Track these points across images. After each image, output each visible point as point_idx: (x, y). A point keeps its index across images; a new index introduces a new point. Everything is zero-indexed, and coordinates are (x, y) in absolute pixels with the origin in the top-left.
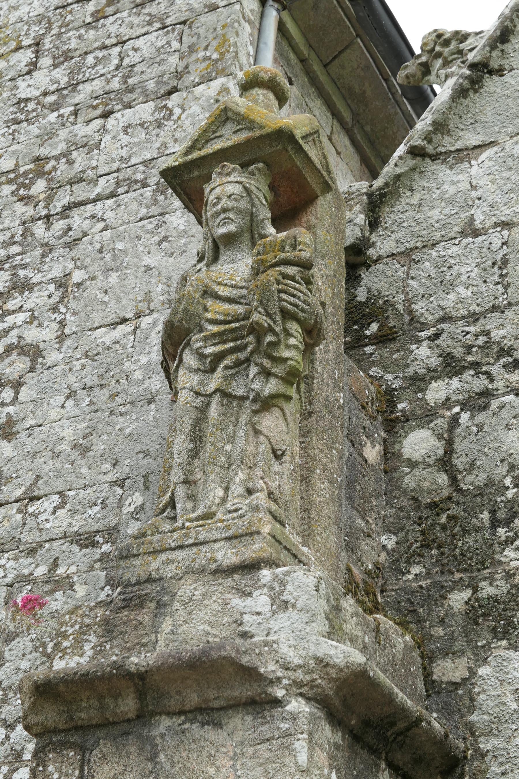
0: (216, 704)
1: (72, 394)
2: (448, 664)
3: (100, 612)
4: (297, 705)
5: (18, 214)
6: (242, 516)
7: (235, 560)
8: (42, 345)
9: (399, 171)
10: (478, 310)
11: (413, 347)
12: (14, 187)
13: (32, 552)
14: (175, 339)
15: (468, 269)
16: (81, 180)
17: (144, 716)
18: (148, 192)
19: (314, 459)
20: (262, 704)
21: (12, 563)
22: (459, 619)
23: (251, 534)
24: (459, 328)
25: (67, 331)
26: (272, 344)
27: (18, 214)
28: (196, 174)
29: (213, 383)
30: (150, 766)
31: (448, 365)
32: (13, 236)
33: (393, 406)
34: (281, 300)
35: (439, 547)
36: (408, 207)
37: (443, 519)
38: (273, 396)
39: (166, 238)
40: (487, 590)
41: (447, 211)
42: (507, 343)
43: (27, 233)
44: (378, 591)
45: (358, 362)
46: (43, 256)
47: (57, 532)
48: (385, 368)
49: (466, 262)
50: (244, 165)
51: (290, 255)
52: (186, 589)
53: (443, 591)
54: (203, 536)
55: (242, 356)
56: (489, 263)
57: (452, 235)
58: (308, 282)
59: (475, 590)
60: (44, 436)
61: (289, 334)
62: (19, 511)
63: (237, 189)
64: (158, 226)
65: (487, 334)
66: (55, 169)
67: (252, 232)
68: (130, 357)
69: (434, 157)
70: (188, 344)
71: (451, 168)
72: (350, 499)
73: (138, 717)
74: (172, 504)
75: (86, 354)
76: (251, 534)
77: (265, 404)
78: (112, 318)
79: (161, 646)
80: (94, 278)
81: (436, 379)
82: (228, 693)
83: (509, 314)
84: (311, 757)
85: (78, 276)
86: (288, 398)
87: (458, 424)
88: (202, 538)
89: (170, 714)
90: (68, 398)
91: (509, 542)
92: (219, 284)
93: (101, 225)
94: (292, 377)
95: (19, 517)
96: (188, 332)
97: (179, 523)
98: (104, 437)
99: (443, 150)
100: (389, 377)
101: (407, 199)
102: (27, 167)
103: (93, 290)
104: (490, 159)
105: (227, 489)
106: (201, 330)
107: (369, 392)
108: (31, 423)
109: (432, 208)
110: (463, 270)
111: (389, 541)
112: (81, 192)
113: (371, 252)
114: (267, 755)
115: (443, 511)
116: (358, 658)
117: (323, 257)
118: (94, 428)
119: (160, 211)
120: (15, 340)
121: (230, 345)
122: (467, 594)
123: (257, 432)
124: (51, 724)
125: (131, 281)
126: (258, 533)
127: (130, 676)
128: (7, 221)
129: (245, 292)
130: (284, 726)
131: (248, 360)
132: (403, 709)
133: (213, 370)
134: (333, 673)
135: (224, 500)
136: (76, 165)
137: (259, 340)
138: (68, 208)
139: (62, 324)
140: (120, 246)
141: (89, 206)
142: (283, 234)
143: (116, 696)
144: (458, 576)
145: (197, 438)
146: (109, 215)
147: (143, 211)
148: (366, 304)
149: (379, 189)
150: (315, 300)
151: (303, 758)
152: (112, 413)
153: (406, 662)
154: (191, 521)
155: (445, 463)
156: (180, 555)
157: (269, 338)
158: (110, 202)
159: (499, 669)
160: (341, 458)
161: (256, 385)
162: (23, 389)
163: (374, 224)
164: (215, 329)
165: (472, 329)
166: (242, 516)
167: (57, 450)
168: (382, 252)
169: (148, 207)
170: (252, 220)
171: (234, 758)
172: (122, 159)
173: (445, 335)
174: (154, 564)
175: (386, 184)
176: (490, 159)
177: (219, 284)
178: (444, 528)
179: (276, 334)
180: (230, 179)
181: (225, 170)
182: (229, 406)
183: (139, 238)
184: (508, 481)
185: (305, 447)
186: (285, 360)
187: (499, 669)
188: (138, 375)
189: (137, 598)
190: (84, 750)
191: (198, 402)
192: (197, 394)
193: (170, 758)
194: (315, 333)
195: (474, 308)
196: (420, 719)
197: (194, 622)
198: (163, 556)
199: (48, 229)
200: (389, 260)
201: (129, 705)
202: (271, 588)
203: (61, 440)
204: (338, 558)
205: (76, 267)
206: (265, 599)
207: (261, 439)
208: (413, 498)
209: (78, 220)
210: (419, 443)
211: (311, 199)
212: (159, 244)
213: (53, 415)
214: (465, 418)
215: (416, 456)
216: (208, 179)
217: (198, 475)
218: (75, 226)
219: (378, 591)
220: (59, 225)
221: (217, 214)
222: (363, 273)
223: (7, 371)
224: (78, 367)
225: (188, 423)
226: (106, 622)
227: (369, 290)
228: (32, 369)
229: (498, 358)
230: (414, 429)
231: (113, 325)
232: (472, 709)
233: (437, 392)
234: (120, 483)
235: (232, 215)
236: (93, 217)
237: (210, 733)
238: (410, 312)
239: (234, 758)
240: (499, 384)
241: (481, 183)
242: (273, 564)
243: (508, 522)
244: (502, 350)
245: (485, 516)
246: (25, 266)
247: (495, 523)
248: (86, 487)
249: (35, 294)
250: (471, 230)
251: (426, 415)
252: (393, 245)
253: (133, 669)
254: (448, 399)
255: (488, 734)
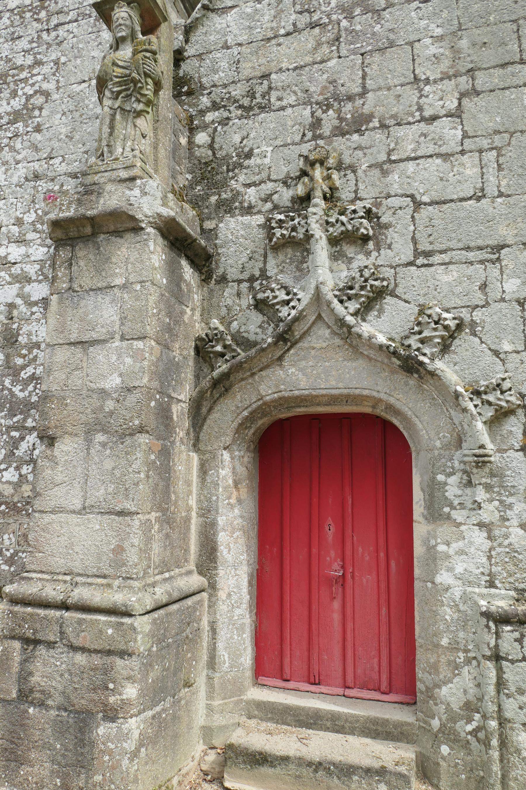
0: (121, 230)
1: (64, 114)
2: (209, 222)
3: (76, 196)
4: (150, 230)
5: (34, 27)
6: (129, 159)
7: (127, 176)
8: (50, 91)
9: (198, 16)
10: (227, 82)
11: (201, 97)
12: (32, 14)
13: (52, 180)
14: (102, 84)
15: (224, 64)
16: (62, 12)
17: (94, 234)
18: (92, 20)
19: (159, 140)
20: (137, 229)
21: (45, 184)
22: (213, 206)
23: (133, 166)
24: (219, 90)
25: (60, 85)
26: (141, 88)
27: (34, 27)
28: (108, 6)
29: (117, 104)
30: (97, 252)
31: (214, 106)
32: (33, 39)
33: (192, 122)
34: (144, 68)
35: (207, 179)
36: (201, 34)
37: (209, 169)
38: (142, 111)
39: (100, 43)
40: (224, 196)
41: (217, 37)
42: (237, 97)
43: (39, 37)
44: (184, 196)
45: (179, 103)
46: (47, 49)
47: (62, 172)
48: (190, 106)
49: (223, 60)
50: (129, 4)
51: (147, 47)
52: (109, 187)
53: (208, 196)
54: (115, 167)
55: (129, 92)
56: (232, 62)
57: (218, 48)
58: (156, 61)
59: (220, 196)
60: (54, 132)
61: (147, 84)
62: (46, 163)
63: (125, 15)
64: (97, 37)
65: (230, 93)
66: (49, 5)
67: (133, 36)
68: (87, 98)
69: (213, 11)
70: (107, 87)
71: (219, 17)
72: (174, 158)
73: (92, 234)
74: (102, 154)
75: (69, 96)
76: (133, 166)
77: (139, 114)
78: (79, 80)
79: (100, 208)
80: (70, 61)
81: (209, 111)
82: (125, 225)
83: (239, 85)
84: (155, 248)
85: (63, 59)
86: (148, 113)
87: (217, 131)
88: (114, 167)
89: (104, 233)
90: (62, 115)
91: (233, 178)
92: (119, 60)
93: (72, 35)
94: (149, 103)
95: (46, 165)
96: (107, 81)
97: (105, 162)
98: (79, 133)
99: (217, 7)
100: (191, 110)
101: (201, 30)
102: (36, 4)
103: (70, 66)
104: (235, 13)
105: (124, 149)
106: (112, 80)
107: (183, 115)
108: (48, 126)
109: (211, 35)
110: (222, 64)
111: (189, 177)
112: (62, 18)
113: (185, 54)
114: (139, 247)
115: (210, 165)
116: (172, 214)
117: (163, 52)
118: (75, 129)
119: (97, 30)
120: (38, 88)
121: (123, 87)
122: (216, 197)
123: (135, 126)
124: (60, 237)
125: (86, 63)
126: (135, 166)
127: (88, 218)
128: (30, 31)
129: (129, 64)
130: (145, 237)
131: (131, 95)
132: (189, 235)
133: (116, 98)
134: (163, 219)
135: (123, 153)
136: (59, 4)
137: (135, 86)
138: (57, 26)
139: (58, 81)
140: (81, 46)
141: (66, 26)
142: (145, 37)
143: (84, 227)
144: (214, 190)
145: (112, 127)
146: (75, 30)
147: (90, 30)
148: (182, 78)
149: (189, 24)
150: (159, 70)
151: (152, 248)
152: (81, 123)
153: (193, 221)
154: (110, 161)
155: (211, 146)
156: (106, 174)
157: (139, 85)
158: (75, 24)
159: (226, 224)
160: (170, 141)
161: (134, 106)
162: (43, 110)
163: (187, 41)
164: (117, 80)
165: (224, 91)
166: (129, 159)
167: (60, 138)
168: (190, 54)
169: (92, 28)
170: (132, 31)
171: (128, 248)
172: (80, 3)
173: (213, 93)
174: (96, 178)
175: (192, 22)
176: (235, 13)
177: (119, 60)
178: (209, 172)
179: (142, 83)
180: (122, 10)
181: (120, 5)
182: (124, 114)
183: (89, 42)
184: (234, 154)
185: (156, 135)
186: (146, 95)
187: (226, 224)
188: (91, 106)
189: (90, 192)
190: (73, 246)
191: (112, 112)
192: (111, 108)
193: (104, 249)
194: (158, 84)
195: (225, 82)
196: (196, 239)
197: (112, 199)
198: (99, 175)
199: (48, 36)
200: (193, 58)
201: (88, 230)
202: (141, 187)
203: (61, 134)
204: (168, 180)
205: (62, 55)
206: (138, 191)
207: (137, 129)
208: (199, 160)
209: (61, 32)
210: (202, 138)
211: (158, 25)
212: (98, 46)
213: (57, 122)
214: (219, 128)
215: (200, 143)
216: (113, 9)
217: (112, 143)
218: (60, 35)
219: (184, 196)
220: (53, 34)
221: (117, 26)
222: (182, 64)
223: (36, 102)
224: (66, 102)
225: (107, 121)
226: (78, 200)
227: (184, 71)
228: (46, 102)
229: (233, 104)
230: (199, 132)
231: (80, 83)
232: (216, 238)
233: (209, 117)
234: (86, 152)
235: (123, 27)
236: (68, 31)
237: (118, 240)
238: (200, 82)
239: (128, 248)
240: (233, 115)
241: (231, 25)
242: (141, 178)
243: (233, 170)
244: (235, 100)
245: (225, 168)
246: (40, 53)
247: (228, 171)
248: (72, 154)
249: (45, 67)
250: (226, 46)
251: (205, 127)
252: (194, 51)
253: (89, 216)
254: (213, 120)
255: (222, 247)
